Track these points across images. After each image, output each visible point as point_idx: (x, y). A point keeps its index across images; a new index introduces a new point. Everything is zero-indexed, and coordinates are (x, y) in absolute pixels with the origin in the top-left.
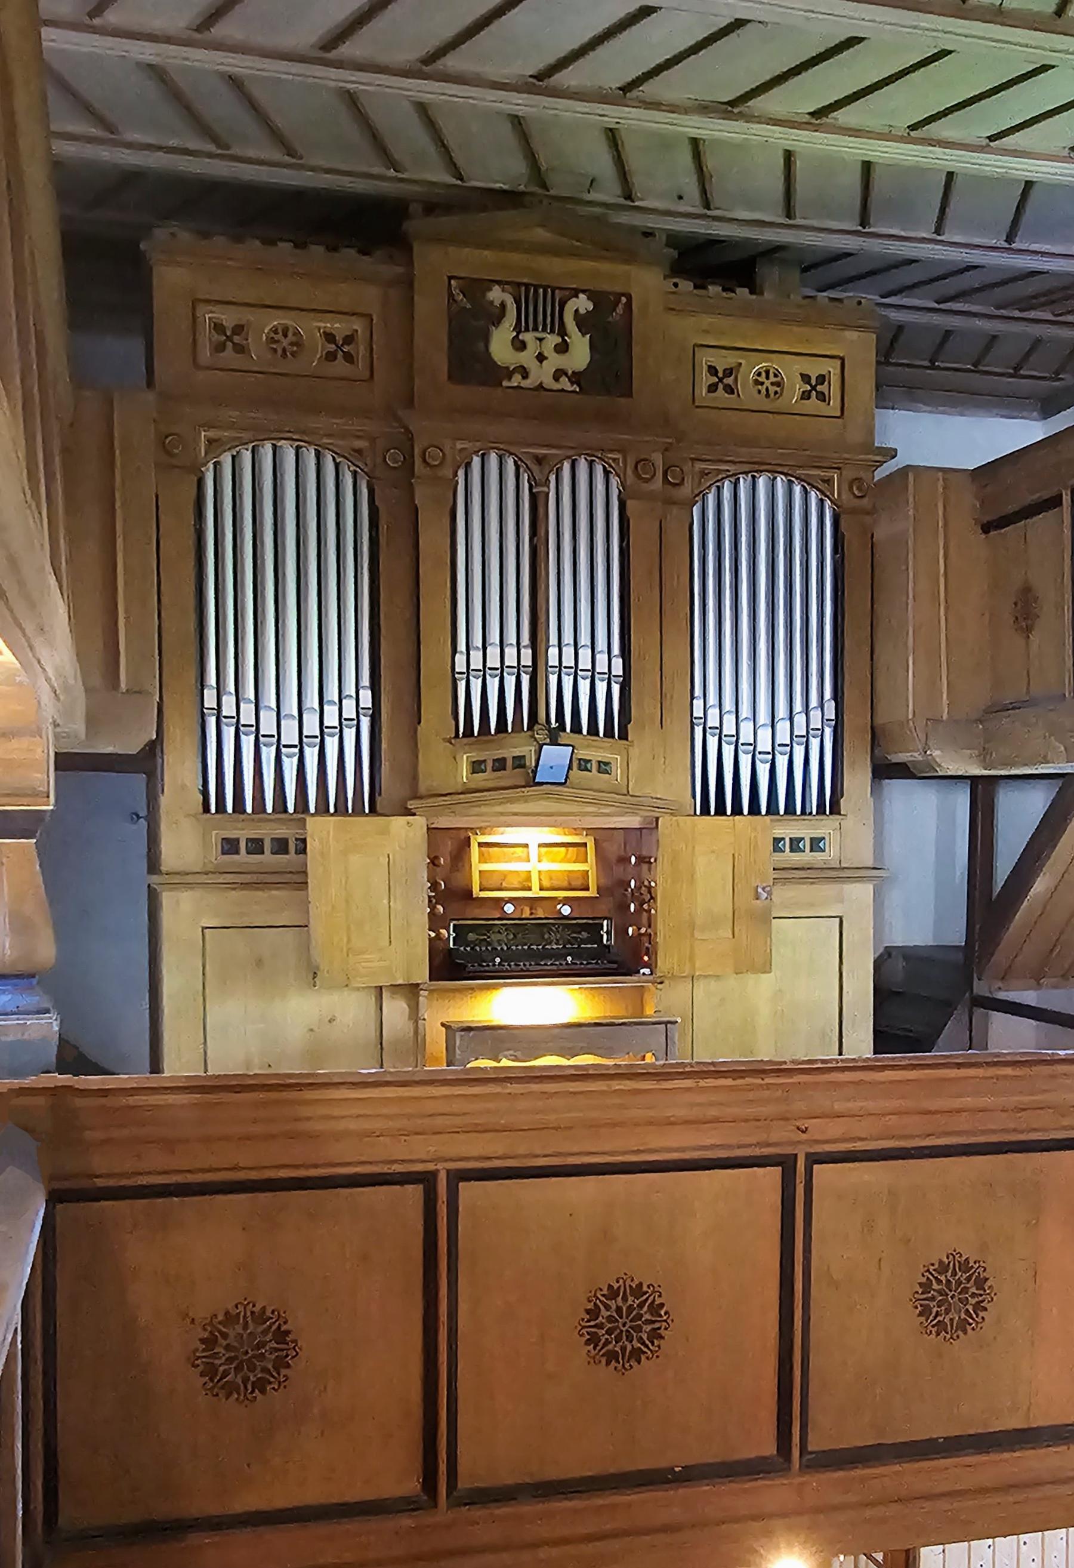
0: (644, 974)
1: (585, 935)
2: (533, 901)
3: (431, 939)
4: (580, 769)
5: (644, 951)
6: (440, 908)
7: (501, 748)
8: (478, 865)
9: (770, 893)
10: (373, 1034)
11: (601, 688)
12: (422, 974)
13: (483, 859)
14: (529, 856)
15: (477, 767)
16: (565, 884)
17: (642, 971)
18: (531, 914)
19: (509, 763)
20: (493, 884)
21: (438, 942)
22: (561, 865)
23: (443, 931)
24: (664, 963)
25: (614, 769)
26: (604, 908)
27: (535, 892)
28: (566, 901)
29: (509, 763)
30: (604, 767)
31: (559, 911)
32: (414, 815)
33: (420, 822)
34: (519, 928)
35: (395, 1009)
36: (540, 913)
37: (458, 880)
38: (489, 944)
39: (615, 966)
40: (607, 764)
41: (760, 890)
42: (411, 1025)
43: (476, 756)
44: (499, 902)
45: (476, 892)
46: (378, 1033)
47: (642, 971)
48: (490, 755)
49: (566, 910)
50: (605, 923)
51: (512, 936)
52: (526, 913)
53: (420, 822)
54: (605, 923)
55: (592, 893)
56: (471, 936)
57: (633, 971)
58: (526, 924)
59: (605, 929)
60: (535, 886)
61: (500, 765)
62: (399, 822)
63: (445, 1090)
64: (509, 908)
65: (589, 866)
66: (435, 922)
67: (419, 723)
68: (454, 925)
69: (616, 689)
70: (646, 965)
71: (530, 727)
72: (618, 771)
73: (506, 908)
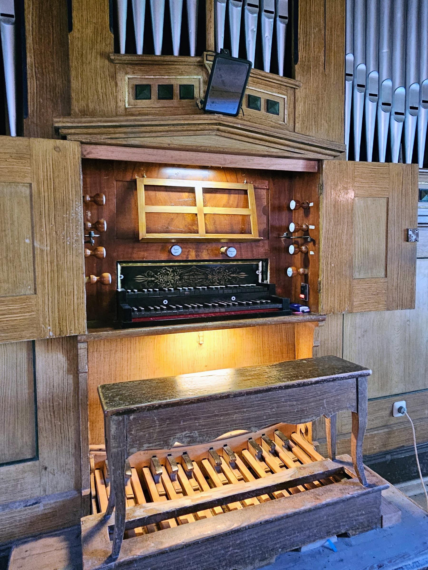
0: (303, 312)
1: (243, 275)
2: (199, 243)
3: (89, 284)
4: (249, 106)
5: (299, 290)
6: (103, 251)
7: (169, 74)
8: (145, 207)
9: (417, 235)
10: (25, 391)
11: (267, 23)
12: (79, 324)
13: (149, 202)
14: (193, 200)
15: (141, 91)
16: (228, 228)
17: (301, 308)
18: (197, 256)
19: (177, 91)
20: (159, 227)
21: (103, 287)
22: (223, 208)
23: (108, 276)
24: (326, 301)
25: (281, 110)
26: (262, 250)
27: (202, 235)
28: (231, 242)
29: (177, 91)
30: (272, 106)
31: (225, 254)
32: (64, 138)
33: (72, 149)
34: (188, 270)
35: (51, 365)
36: (205, 256)
37: (125, 225)
38: (156, 286)
39: (280, 306)
40: (276, 104)
41: (410, 233)
42: (70, 379)
43: (139, 78)
44: (166, 244)
45: (143, 234)
46: (32, 390)
47: (301, 308)
48: (155, 79)
49: (232, 252)
50: (260, 264)
51: (178, 278)
52: (192, 256)
53: (72, 149)
54: (260, 264)
55: (254, 235)
56: (140, 278)
57: (293, 311)
58: (191, 266)
59: (260, 268)
60: (202, 228)
61: (166, 92)
62: (43, 146)
63: (162, 123)
64: (177, 251)
65: (251, 211)
66: (94, 264)
67: (70, 28)
68: (122, 268)
69: (281, 27)
70: (305, 303)
71: (199, 53)
72: (284, 111)
73: (173, 251)
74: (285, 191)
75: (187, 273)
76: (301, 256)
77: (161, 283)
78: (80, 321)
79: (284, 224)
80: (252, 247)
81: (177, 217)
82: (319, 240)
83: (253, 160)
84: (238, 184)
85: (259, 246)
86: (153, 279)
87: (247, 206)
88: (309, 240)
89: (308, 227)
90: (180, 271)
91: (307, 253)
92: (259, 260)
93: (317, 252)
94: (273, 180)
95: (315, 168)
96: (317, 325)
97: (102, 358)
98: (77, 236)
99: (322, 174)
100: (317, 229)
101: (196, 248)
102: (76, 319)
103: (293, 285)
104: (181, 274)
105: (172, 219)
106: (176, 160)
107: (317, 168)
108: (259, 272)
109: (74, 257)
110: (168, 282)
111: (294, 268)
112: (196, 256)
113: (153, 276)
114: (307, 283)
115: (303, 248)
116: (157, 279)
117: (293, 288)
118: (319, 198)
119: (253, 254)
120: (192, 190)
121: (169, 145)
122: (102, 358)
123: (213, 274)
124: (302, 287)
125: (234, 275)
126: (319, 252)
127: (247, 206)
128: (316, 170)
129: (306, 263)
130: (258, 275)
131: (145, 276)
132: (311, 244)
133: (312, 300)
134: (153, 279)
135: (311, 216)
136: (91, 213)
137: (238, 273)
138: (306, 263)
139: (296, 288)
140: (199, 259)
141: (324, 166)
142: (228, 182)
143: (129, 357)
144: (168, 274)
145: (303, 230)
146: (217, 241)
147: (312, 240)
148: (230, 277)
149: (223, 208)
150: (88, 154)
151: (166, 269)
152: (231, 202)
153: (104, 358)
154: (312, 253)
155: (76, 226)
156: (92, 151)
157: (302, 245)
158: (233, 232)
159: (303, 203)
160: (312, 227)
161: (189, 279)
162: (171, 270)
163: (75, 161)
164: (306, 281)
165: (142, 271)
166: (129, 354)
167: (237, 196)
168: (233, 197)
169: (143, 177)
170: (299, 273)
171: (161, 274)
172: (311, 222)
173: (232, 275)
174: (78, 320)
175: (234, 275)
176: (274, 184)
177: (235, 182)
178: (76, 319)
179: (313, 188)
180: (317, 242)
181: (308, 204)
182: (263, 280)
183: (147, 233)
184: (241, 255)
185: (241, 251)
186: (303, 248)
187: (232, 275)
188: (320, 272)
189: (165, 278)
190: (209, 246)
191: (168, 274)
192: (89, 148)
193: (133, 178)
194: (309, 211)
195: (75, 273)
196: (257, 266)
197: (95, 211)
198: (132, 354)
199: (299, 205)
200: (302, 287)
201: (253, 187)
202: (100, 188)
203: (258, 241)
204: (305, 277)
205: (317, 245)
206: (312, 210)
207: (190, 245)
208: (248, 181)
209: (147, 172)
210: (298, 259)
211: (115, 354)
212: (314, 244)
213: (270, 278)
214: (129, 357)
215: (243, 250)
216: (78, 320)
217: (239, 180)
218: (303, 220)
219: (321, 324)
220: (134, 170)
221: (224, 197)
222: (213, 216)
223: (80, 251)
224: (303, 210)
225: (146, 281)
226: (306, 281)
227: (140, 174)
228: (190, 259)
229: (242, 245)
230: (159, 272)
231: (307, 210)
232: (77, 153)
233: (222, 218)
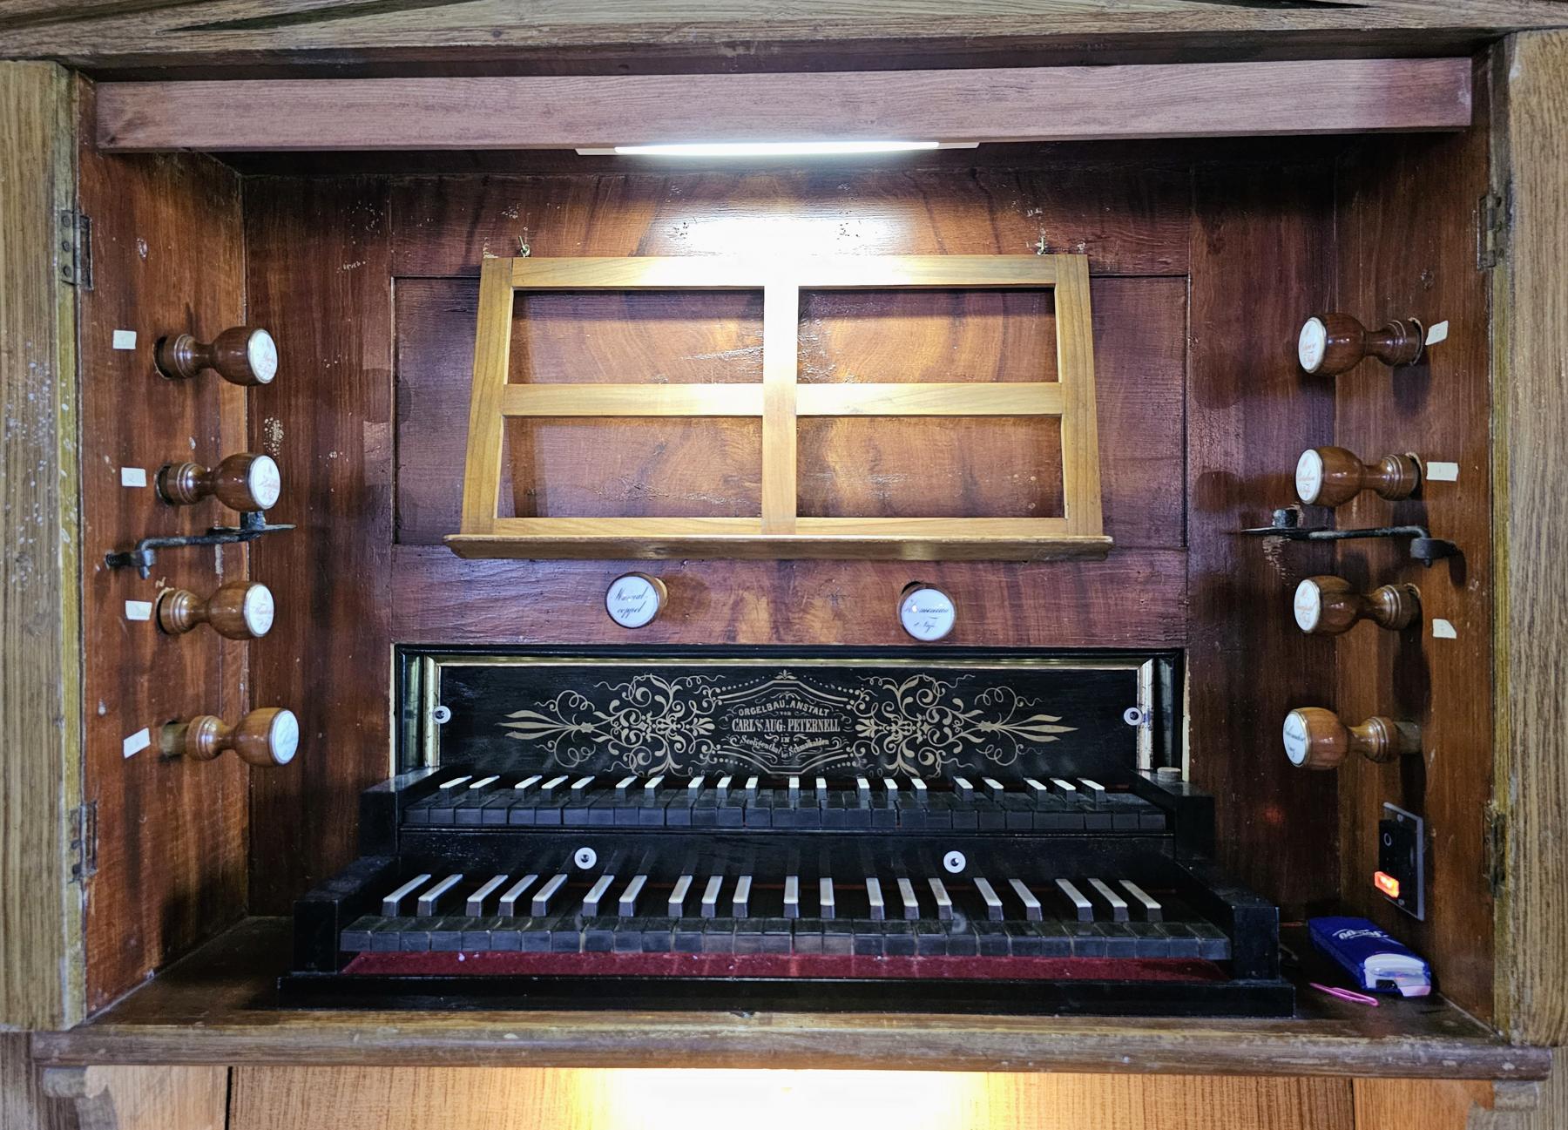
0: (1387, 990)
1: (1048, 728)
5: (1371, 840)
22: (894, 387)
28: (944, 566)
36: (820, 627)
51: (704, 726)
54: (1146, 670)
55: (1078, 524)
56: (525, 723)
58: (772, 673)
65: (1064, 388)
68: (447, 675)
74: (1283, 278)
75: (750, 704)
76: (1383, 642)
77: (623, 750)
78: (37, 961)
79: (1274, 463)
80: (1081, 588)
81: (685, 437)
82: (1490, 548)
83: (1021, 89)
84: (998, 260)
85: (1124, 581)
86: (587, 728)
87: (1050, 374)
88: (1418, 548)
89: (1421, 474)
90: (715, 697)
91: (1413, 625)
92: (1139, 656)
93: (1481, 625)
94: (1211, 227)
95: (1454, 101)
96: (1489, 1103)
97: (295, 1100)
98: (33, 530)
99: (1504, 127)
100: (1479, 478)
101: (775, 588)
102: (17, 947)
103: (1344, 799)
104: (721, 710)
105: (662, 447)
106: (569, 127)
107: (1467, 100)
108: (1139, 716)
109: (15, 634)
110: (656, 744)
111: (1320, 715)
112: (775, 627)
113: (587, 716)
114: (1419, 811)
115: (1388, 597)
116: (607, 728)
117: (1344, 822)
118: (1484, 281)
119: (1091, 624)
120: (749, 301)
121: (497, 33)
122: (295, 1100)
123: (880, 717)
124: (1386, 826)
125: (997, 727)
126: (1490, 627)
127: (1050, 374)
128: (1460, 113)
129: (1410, 685)
130: (1134, 731)
131: (553, 716)
132: (1439, 573)
133: (1447, 927)
134: (587, 728)
135: (1433, 405)
136: (286, 427)
137: (1022, 715)
138: (1410, 685)
139: (1356, 824)
140: (789, 640)
141: (1515, 73)
142: (943, 251)
143: (420, 1112)
144: (657, 709)
145: (1384, 492)
146: (883, 554)
147: (1443, 551)
148: (978, 734)
149: (894, 387)
150: (130, 126)
151: (648, 683)
152: (964, 357)
153: (305, 1104)
154: (1443, 629)
155: (26, 480)
156: (149, 111)
157: (1386, 578)
158: (971, 509)
159: (1387, 332)
160: (1442, 471)
161: (759, 735)
162: (672, 689)
163: (28, 155)
164: (1413, 796)
165: (534, 689)
166: (420, 1101)
167: (998, 321)
168: (981, 333)
169: (518, 253)
170: (1356, 749)
171: (624, 704)
172: (1434, 441)
173: (986, 726)
174: (26, 954)
175: (997, 727)
176: (1214, 248)
177: (986, 250)
178: (17, 947)
179: (1449, 230)
180: (1476, 563)
181: (1419, 331)
182: (1158, 760)
183: (799, 515)
184: (1019, 623)
185: (1017, 607)
186: (1388, 597)
187: (986, 726)
188: (1501, 759)
189: (646, 725)
190: (844, 576)
191: (657, 709)
192: (126, 100)
193: (473, 260)
194: (1427, 377)
195: (16, 714)
196: (1131, 680)
197: (301, 420)
198: (437, 1101)
199: (1358, 350)
200: (1386, 826)
201: (1084, 270)
202: (326, 312)
203: (1097, 552)
204: (1406, 767)
205: (1474, 585)
206: (1439, 367)
207: (744, 574)
208: (1060, 240)
209: (535, 226)
210: (1365, 655)
211: (355, 1086)
212: (1459, 577)
213: (1193, 754)
214: (420, 1112)
215: (1028, 603)
216: (26, 954)
217: (1009, 238)
218: (1389, 434)
219: (1509, 1095)
220: (476, 220)
221: (933, 329)
222: (864, 428)
223: (44, 604)
224: (1390, 371)
225: (554, 736)
226: (1413, 796)
227: (504, 243)
228: (743, 640)
229: (1022, 574)
230: (618, 695)
231: (1411, 374)
232: (36, 118)
233: (914, 437)
